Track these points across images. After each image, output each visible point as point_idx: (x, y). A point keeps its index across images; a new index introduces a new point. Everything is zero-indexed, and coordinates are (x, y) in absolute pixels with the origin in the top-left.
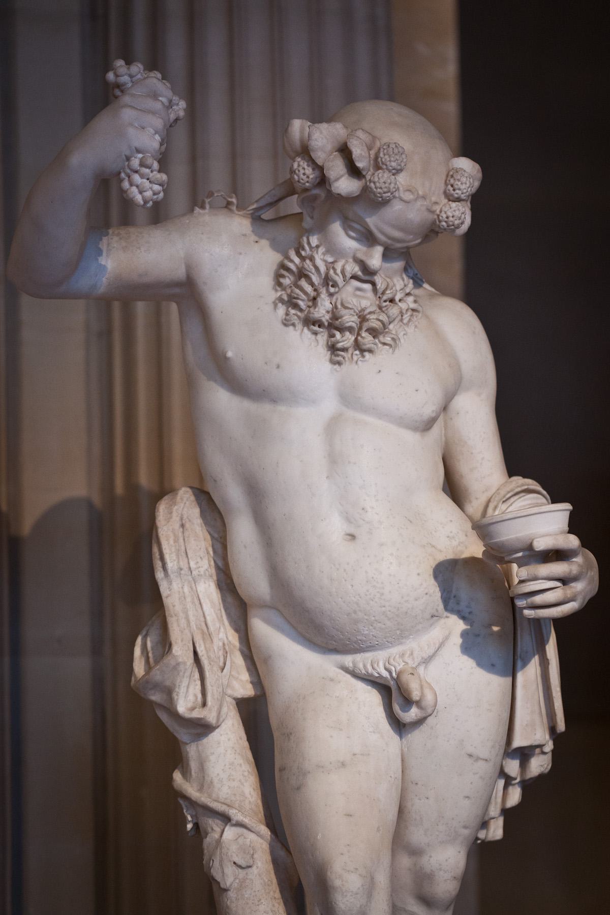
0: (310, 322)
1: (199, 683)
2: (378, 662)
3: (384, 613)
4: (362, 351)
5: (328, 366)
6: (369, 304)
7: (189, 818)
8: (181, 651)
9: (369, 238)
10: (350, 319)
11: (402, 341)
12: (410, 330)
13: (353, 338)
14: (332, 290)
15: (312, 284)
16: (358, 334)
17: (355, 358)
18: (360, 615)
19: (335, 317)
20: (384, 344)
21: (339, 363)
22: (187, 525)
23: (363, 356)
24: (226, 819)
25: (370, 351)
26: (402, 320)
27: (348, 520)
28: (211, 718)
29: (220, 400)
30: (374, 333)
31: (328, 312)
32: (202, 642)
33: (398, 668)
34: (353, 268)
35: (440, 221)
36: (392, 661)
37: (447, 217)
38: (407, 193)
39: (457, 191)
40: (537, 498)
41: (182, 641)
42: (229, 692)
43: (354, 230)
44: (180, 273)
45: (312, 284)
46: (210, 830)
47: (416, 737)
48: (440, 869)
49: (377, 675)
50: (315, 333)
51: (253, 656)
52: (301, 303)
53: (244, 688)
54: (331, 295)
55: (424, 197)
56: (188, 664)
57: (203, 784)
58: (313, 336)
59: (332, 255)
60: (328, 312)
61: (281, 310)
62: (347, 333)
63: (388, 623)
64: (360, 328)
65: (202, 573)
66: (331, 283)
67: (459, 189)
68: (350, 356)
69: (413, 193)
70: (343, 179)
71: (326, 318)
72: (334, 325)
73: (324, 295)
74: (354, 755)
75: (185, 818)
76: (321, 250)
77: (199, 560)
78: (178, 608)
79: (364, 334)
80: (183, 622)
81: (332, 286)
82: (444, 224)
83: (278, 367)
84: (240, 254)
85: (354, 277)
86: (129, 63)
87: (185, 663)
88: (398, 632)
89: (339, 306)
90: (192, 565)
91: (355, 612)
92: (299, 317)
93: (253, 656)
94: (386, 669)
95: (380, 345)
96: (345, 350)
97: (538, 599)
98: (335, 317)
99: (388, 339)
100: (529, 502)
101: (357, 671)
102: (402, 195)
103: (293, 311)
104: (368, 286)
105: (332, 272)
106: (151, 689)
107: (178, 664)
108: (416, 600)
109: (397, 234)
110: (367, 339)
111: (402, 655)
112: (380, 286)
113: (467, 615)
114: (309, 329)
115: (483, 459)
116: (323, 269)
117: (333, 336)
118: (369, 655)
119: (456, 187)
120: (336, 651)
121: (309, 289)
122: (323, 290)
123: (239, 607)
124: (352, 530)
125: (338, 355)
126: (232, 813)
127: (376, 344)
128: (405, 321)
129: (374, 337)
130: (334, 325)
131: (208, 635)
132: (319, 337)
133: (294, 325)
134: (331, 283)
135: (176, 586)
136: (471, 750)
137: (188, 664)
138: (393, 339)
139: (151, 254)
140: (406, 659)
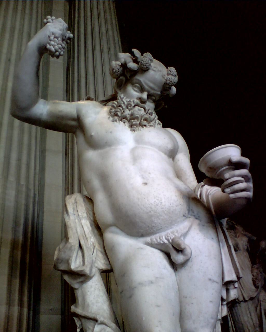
0: (123, 118)
1: (81, 257)
2: (163, 237)
3: (163, 212)
7: (78, 326)
8: (73, 241)
9: (142, 90)
14: (129, 108)
17: (140, 129)
18: (153, 213)
21: (134, 131)
22: (78, 202)
24: (96, 320)
25: (145, 126)
27: (143, 178)
28: (87, 271)
33: (172, 238)
35: (167, 81)
36: (168, 235)
37: (169, 79)
39: (171, 72)
42: (96, 265)
43: (136, 87)
46: (88, 329)
47: (184, 272)
49: (162, 243)
50: (124, 123)
51: (107, 250)
53: (101, 264)
57: (85, 306)
58: (124, 124)
62: (136, 120)
63: (165, 217)
67: (172, 72)
75: (76, 326)
78: (72, 225)
80: (74, 231)
81: (130, 107)
87: (74, 246)
88: (170, 221)
90: (80, 214)
93: (107, 250)
94: (166, 239)
96: (136, 125)
97: (236, 187)
101: (153, 243)
106: (60, 263)
107: (71, 247)
109: (152, 85)
110: (145, 122)
111: (173, 233)
113: (198, 218)
116: (126, 103)
118: (157, 235)
119: (171, 70)
120: (142, 236)
123: (99, 229)
124: (145, 181)
126: (98, 317)
131: (86, 238)
132: (126, 123)
133: (116, 121)
135: (72, 217)
136: (210, 277)
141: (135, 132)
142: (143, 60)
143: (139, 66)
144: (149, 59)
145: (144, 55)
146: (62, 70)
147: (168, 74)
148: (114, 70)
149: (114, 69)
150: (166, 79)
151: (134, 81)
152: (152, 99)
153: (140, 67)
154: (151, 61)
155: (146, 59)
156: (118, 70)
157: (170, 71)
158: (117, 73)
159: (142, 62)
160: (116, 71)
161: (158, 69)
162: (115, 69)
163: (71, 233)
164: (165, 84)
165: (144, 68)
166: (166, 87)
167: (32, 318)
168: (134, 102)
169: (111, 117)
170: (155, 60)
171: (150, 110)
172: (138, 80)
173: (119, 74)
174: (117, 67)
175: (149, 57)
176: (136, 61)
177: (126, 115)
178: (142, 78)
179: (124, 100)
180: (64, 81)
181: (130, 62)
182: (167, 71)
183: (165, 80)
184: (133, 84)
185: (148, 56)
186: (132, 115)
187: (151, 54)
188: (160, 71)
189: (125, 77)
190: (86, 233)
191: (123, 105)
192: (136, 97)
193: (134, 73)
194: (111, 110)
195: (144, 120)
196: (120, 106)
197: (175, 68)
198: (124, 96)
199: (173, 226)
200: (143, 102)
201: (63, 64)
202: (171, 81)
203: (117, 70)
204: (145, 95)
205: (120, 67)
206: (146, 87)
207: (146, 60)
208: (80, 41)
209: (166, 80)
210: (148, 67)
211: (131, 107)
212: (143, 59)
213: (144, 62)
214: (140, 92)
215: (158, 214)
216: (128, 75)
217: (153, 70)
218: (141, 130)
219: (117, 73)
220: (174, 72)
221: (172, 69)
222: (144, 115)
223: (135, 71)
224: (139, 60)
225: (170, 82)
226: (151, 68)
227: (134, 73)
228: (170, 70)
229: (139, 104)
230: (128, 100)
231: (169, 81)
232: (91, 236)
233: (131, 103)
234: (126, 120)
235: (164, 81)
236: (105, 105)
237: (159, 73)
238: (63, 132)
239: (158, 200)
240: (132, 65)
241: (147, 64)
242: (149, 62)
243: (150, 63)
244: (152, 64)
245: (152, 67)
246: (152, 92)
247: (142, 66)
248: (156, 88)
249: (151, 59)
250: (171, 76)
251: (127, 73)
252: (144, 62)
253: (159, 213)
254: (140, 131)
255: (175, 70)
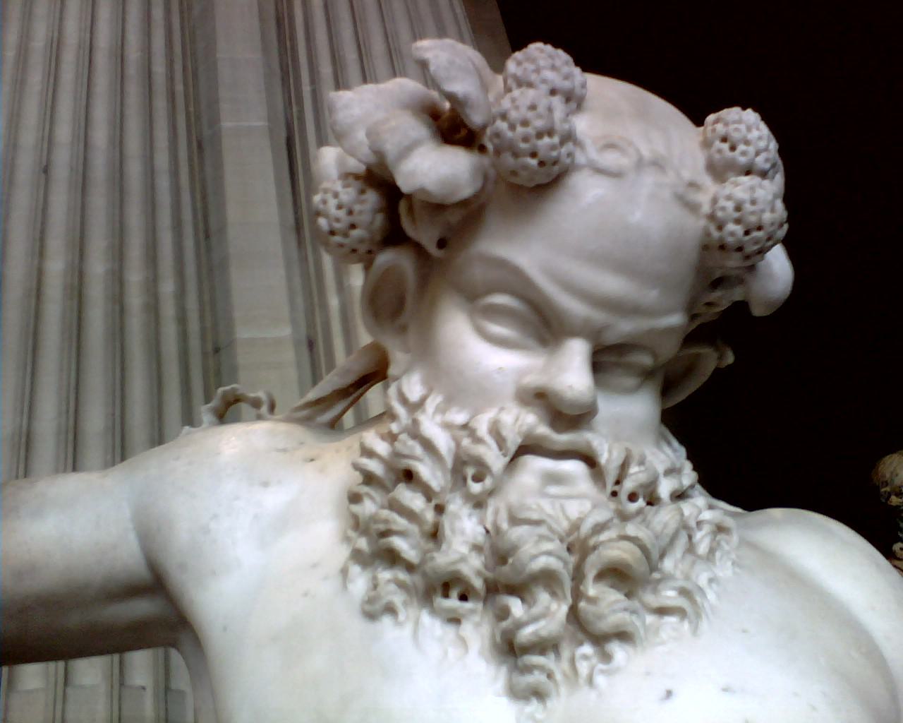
0: (442, 587)
4: (600, 640)
5: (506, 709)
6: (587, 505)
9: (545, 326)
10: (538, 552)
11: (711, 596)
12: (724, 569)
13: (564, 609)
14: (476, 488)
15: (428, 493)
16: (577, 595)
17: (583, 668)
19: (499, 553)
20: (662, 611)
21: (538, 694)
23: (606, 657)
25: (623, 636)
26: (691, 549)
30: (617, 575)
31: (477, 548)
34: (524, 422)
35: (720, 228)
37: (738, 208)
39: (741, 147)
44: (127, 557)
45: (428, 493)
50: (455, 620)
52: (399, 543)
54: (479, 503)
58: (450, 630)
60: (477, 548)
61: (360, 582)
62: (543, 597)
64: (578, 575)
66: (470, 471)
67: (747, 143)
68: (565, 665)
71: (473, 568)
72: (504, 582)
73: (456, 505)
76: (433, 402)
79: (592, 589)
81: (477, 479)
82: (731, 227)
85: (529, 447)
89: (504, 525)
92: (401, 585)
95: (650, 619)
96: (544, 646)
98: (499, 553)
99: (669, 596)
103: (385, 575)
104: (573, 467)
105: (466, 442)
109: (612, 284)
110: (608, 604)
112: (608, 455)
114: (434, 612)
116: (443, 442)
117: (504, 614)
119: (736, 136)
121: (414, 500)
122: (456, 505)
125: (528, 669)
127: (634, 612)
128: (703, 548)
129: (629, 595)
130: (504, 582)
132: (467, 628)
133: (390, 610)
134: (470, 471)
138: (684, 592)
141: (549, 704)
142: (504, 116)
143: (486, 160)
144: (553, 92)
145: (511, 66)
146: (268, 155)
147: (719, 171)
148: (322, 222)
149: (318, 214)
150: (706, 209)
151: (478, 273)
152: (629, 369)
153: (494, 165)
154: (573, 105)
155: (525, 96)
156: (350, 213)
157: (725, 146)
158: (346, 235)
159: (502, 125)
160: (337, 226)
161: (638, 151)
162: (326, 216)
164: (712, 248)
165: (524, 174)
166: (716, 263)
168: (496, 432)
169: (355, 569)
170: (601, 87)
171: (634, 469)
172: (503, 264)
173: (361, 241)
174: (336, 195)
175: (548, 74)
176: (452, 128)
177: (453, 568)
178: (525, 250)
179: (431, 427)
180: (280, 196)
181: (407, 150)
182: (707, 144)
183: (703, 223)
184: (472, 297)
185: (545, 62)
186: (498, 552)
187: (560, 52)
188: (658, 164)
189: (416, 250)
191: (425, 470)
192: (510, 389)
193: (462, 218)
194: (356, 508)
195: (600, 576)
196: (409, 476)
197: (755, 110)
198: (430, 390)
200: (568, 416)
201: (271, 131)
202: (753, 219)
203: (338, 220)
204: (572, 372)
205: (362, 192)
206: (574, 307)
207: (533, 107)
208: (167, 66)
209: (712, 217)
210: (555, 163)
211: (488, 482)
212: (506, 103)
213: (520, 129)
214: (531, 342)
216: (426, 236)
217: (599, 171)
218: (590, 681)
219: (346, 241)
220: (762, 144)
221: (743, 127)
222: (599, 528)
223: (464, 203)
224: (476, 118)
225: (747, 233)
226: (580, 158)
227: (462, 218)
228: (724, 140)
229: (544, 438)
230: (459, 417)
231: (738, 221)
233: (480, 450)
234: (463, 598)
235: (695, 226)
236: (334, 426)
237: (655, 179)
238: (101, 652)
240: (434, 168)
241: (540, 135)
242: (553, 122)
243: (566, 126)
244: (582, 125)
245: (588, 143)
246: (625, 328)
247: (508, 160)
248: (651, 296)
249: (566, 84)
250: (745, 179)
251: (414, 221)
252: (512, 127)
254: (586, 697)
255: (764, 130)
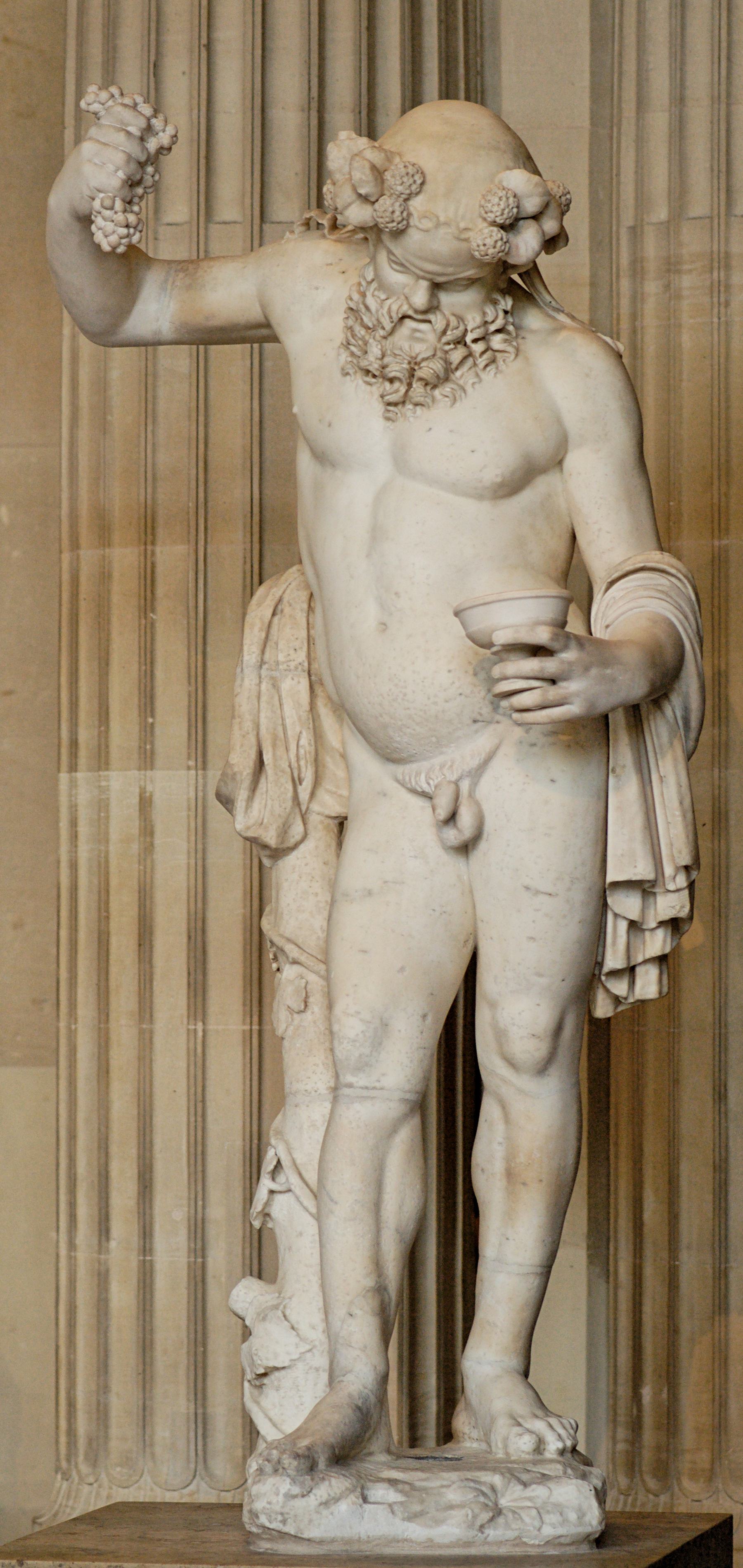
5: (382, 421)
29: (305, 462)
32: (270, 749)
37: (478, 246)
38: (424, 221)
40: (651, 578)
41: (242, 746)
48: (514, 1024)
55: (447, 224)
56: (245, 773)
59: (384, 292)
65: (292, 667)
69: (431, 220)
70: (353, 206)
74: (385, 882)
76: (374, 285)
77: (292, 652)
83: (330, 425)
84: (317, 288)
86: (104, 87)
91: (381, 716)
100: (634, 583)
102: (418, 224)
108: (447, 701)
115: (600, 530)
137: (245, 773)
139: (230, 291)
140: (445, 771)
163: (672, 286)
167: (732, 924)
190: (288, 722)
199: (444, 749)
215: (400, 723)
232: (301, 733)
239: (396, 685)
253: (401, 720)
